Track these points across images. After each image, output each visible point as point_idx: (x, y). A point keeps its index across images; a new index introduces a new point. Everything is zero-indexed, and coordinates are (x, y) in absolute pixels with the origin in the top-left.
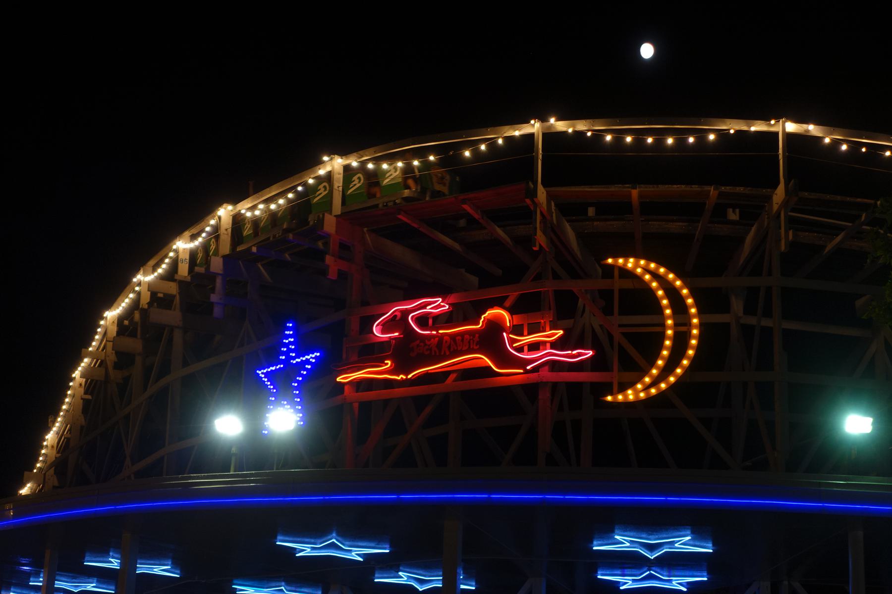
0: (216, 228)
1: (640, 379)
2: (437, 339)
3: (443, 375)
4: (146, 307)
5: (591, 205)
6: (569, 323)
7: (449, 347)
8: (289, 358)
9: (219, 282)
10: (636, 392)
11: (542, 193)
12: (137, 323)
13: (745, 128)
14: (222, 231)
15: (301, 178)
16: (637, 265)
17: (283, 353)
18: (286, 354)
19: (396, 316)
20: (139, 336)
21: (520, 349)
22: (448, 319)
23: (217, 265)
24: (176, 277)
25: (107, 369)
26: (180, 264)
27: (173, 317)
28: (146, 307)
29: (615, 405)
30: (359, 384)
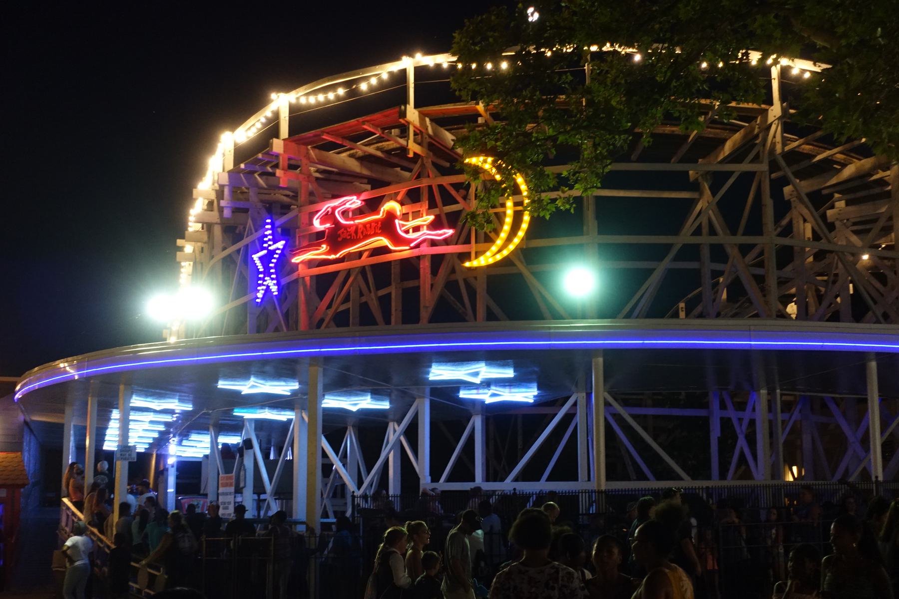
1: (488, 249)
3: (360, 254)
10: (487, 258)
21: (407, 232)
29: (470, 269)
30: (310, 263)
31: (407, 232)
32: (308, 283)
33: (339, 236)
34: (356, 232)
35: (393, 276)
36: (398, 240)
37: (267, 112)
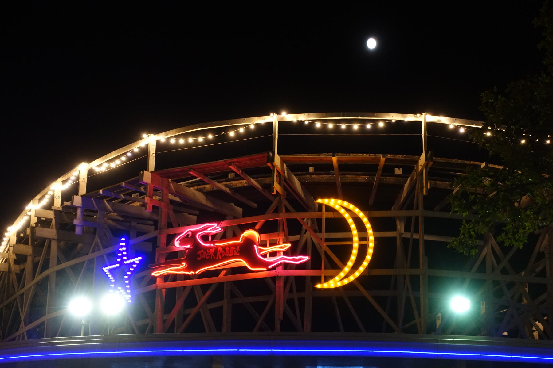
0: (78, 178)
1: (337, 274)
2: (214, 249)
3: (216, 273)
4: (34, 225)
5: (311, 166)
6: (296, 238)
7: (221, 254)
8: (123, 260)
9: (79, 212)
10: (336, 282)
11: (278, 160)
12: (28, 236)
13: (401, 119)
14: (81, 180)
15: (130, 147)
16: (336, 203)
17: (119, 257)
18: (121, 257)
19: (188, 235)
20: (30, 244)
21: (265, 256)
22: (224, 236)
23: (77, 200)
24: (53, 208)
25: (9, 264)
26: (55, 199)
27: (50, 233)
28: (34, 225)
29: (320, 290)
30: (166, 278)
31: (265, 256)
32: (164, 294)
33: (199, 256)
34: (215, 253)
35: (225, 293)
36: (255, 262)
37: (136, 148)
